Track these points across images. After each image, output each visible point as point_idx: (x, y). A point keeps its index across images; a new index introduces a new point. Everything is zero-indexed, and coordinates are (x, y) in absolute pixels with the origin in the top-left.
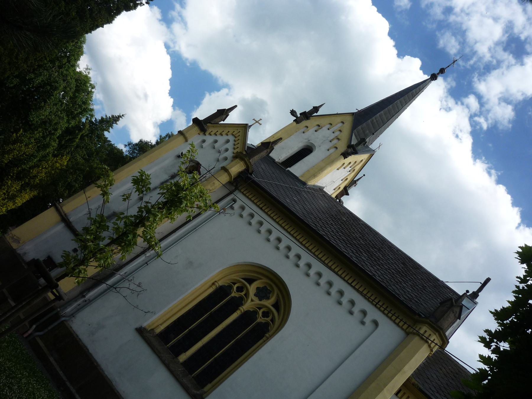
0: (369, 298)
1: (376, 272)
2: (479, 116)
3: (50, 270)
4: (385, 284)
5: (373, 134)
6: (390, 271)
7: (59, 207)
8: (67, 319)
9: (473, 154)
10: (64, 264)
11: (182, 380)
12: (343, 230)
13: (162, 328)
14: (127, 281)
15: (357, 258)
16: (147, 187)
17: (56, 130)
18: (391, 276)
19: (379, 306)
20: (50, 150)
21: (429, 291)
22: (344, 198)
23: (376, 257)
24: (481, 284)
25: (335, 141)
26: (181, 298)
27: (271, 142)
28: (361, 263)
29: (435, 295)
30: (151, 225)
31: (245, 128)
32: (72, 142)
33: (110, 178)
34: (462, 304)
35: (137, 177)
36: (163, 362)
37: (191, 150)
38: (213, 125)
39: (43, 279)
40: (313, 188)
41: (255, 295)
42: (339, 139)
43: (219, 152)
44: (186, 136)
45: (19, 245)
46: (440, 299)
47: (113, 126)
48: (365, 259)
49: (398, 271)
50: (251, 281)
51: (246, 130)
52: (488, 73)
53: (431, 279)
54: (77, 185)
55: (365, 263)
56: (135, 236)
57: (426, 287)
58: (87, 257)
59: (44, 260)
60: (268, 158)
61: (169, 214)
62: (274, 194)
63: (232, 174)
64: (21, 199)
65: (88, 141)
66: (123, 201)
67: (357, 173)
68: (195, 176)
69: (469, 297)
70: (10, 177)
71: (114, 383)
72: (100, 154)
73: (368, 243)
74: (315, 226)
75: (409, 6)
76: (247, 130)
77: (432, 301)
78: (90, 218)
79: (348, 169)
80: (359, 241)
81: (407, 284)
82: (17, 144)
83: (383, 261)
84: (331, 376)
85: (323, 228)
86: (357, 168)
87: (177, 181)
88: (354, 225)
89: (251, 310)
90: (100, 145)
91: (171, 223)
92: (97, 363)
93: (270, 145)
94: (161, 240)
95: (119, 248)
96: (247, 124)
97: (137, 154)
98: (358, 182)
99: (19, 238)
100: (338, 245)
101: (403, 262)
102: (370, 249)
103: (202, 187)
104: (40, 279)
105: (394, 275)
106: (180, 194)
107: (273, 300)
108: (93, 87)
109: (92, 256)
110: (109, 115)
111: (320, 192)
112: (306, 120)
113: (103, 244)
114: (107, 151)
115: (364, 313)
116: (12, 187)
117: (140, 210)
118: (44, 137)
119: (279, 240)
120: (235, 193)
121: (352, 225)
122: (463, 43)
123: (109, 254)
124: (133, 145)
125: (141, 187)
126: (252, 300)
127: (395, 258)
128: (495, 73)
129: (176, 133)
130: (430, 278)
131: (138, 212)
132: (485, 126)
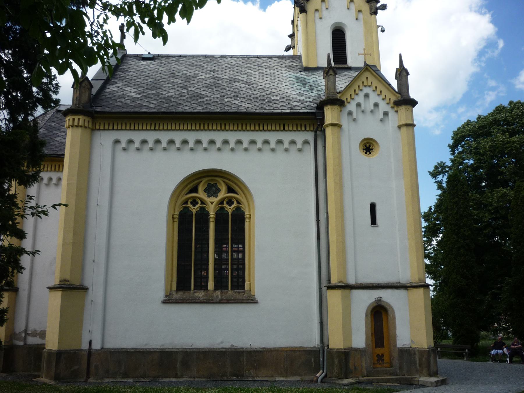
107: (223, 189)
126: (212, 203)
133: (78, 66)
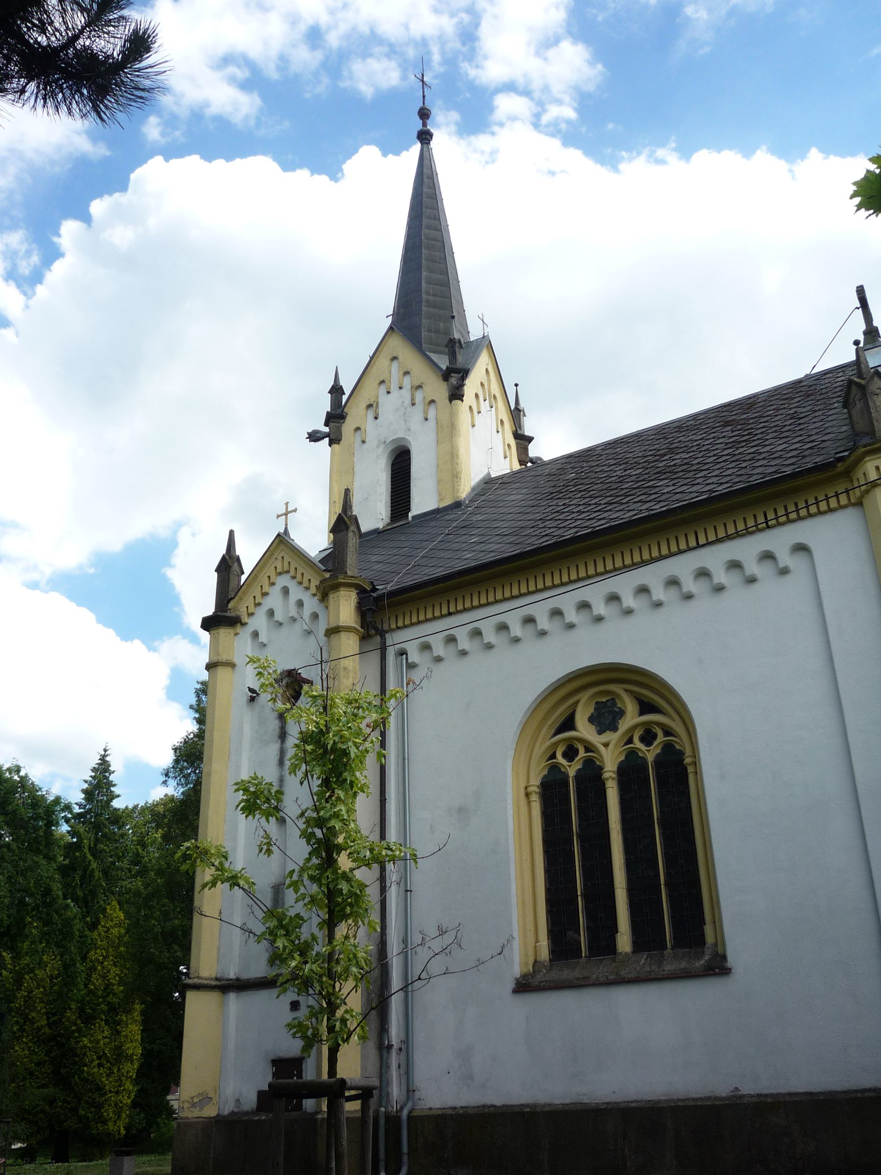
0: (756, 526)
1: (707, 484)
2: (545, 111)
3: (300, 1076)
4: (740, 482)
5: (453, 317)
6: (724, 458)
7: (196, 981)
8: (410, 1105)
9: (605, 167)
10: (311, 1041)
11: (664, 970)
12: (590, 491)
14: (419, 949)
15: (660, 501)
16: (273, 794)
17: (48, 891)
18: (734, 461)
19: (774, 522)
20: (77, 925)
21: (808, 411)
22: (533, 451)
23: (681, 465)
24: (860, 309)
25: (419, 396)
27: (340, 512)
28: (673, 501)
29: (823, 406)
30: (348, 834)
31: (282, 541)
32: (92, 875)
33: (213, 852)
34: (872, 368)
35: (243, 799)
36: (608, 983)
37: (260, 670)
38: (237, 598)
39: (308, 1100)
40: (476, 495)
41: (600, 732)
42: (420, 387)
43: (294, 620)
44: (224, 661)
45: (215, 1103)
46: (837, 402)
47: (112, 781)
48: (672, 488)
49: (732, 442)
50: (568, 724)
51: (288, 545)
52: (477, 44)
53: (788, 393)
54: (177, 922)
55: (679, 493)
56: (347, 878)
57: (796, 412)
58: (328, 991)
59: (274, 1075)
60: (366, 539)
61: (352, 787)
62: (440, 572)
63: (350, 625)
64: (131, 1041)
65: (108, 847)
66: (269, 856)
67: (504, 394)
68: (315, 693)
69: (868, 346)
70: (76, 1035)
71: (586, 1101)
72: (147, 840)
73: (645, 462)
74: (548, 538)
75: (258, 101)
76: (288, 542)
77: (830, 418)
78: (259, 938)
79: (485, 406)
80: (631, 476)
81: (767, 443)
82: (25, 979)
83: (697, 458)
84: (842, 695)
85: (562, 525)
86: (495, 389)
87: (301, 733)
88: (595, 466)
89: (622, 758)
90: (129, 829)
91: (369, 794)
92: (527, 1106)
93: (346, 518)
94: (383, 836)
95: (350, 921)
96: (279, 535)
97: (194, 772)
98: (522, 405)
99: (202, 1093)
100: (611, 519)
101: (722, 423)
102: (658, 467)
103: (342, 695)
104: (304, 1107)
105: (735, 455)
106: (328, 743)
107: (630, 707)
108: (18, 770)
109: (332, 983)
110: (88, 775)
111: (493, 485)
112: (344, 422)
113: (323, 947)
114: (150, 823)
115: (768, 556)
116: (98, 1042)
117: (308, 836)
118: (47, 922)
119: (530, 620)
120: (389, 642)
121: (591, 469)
122: (393, 50)
123: (349, 948)
124: (173, 767)
125: (266, 805)
126: (606, 745)
127: (705, 433)
128: (485, 31)
129: (205, 676)
130: (785, 394)
131: (308, 843)
132: (569, 113)
133: (84, 609)
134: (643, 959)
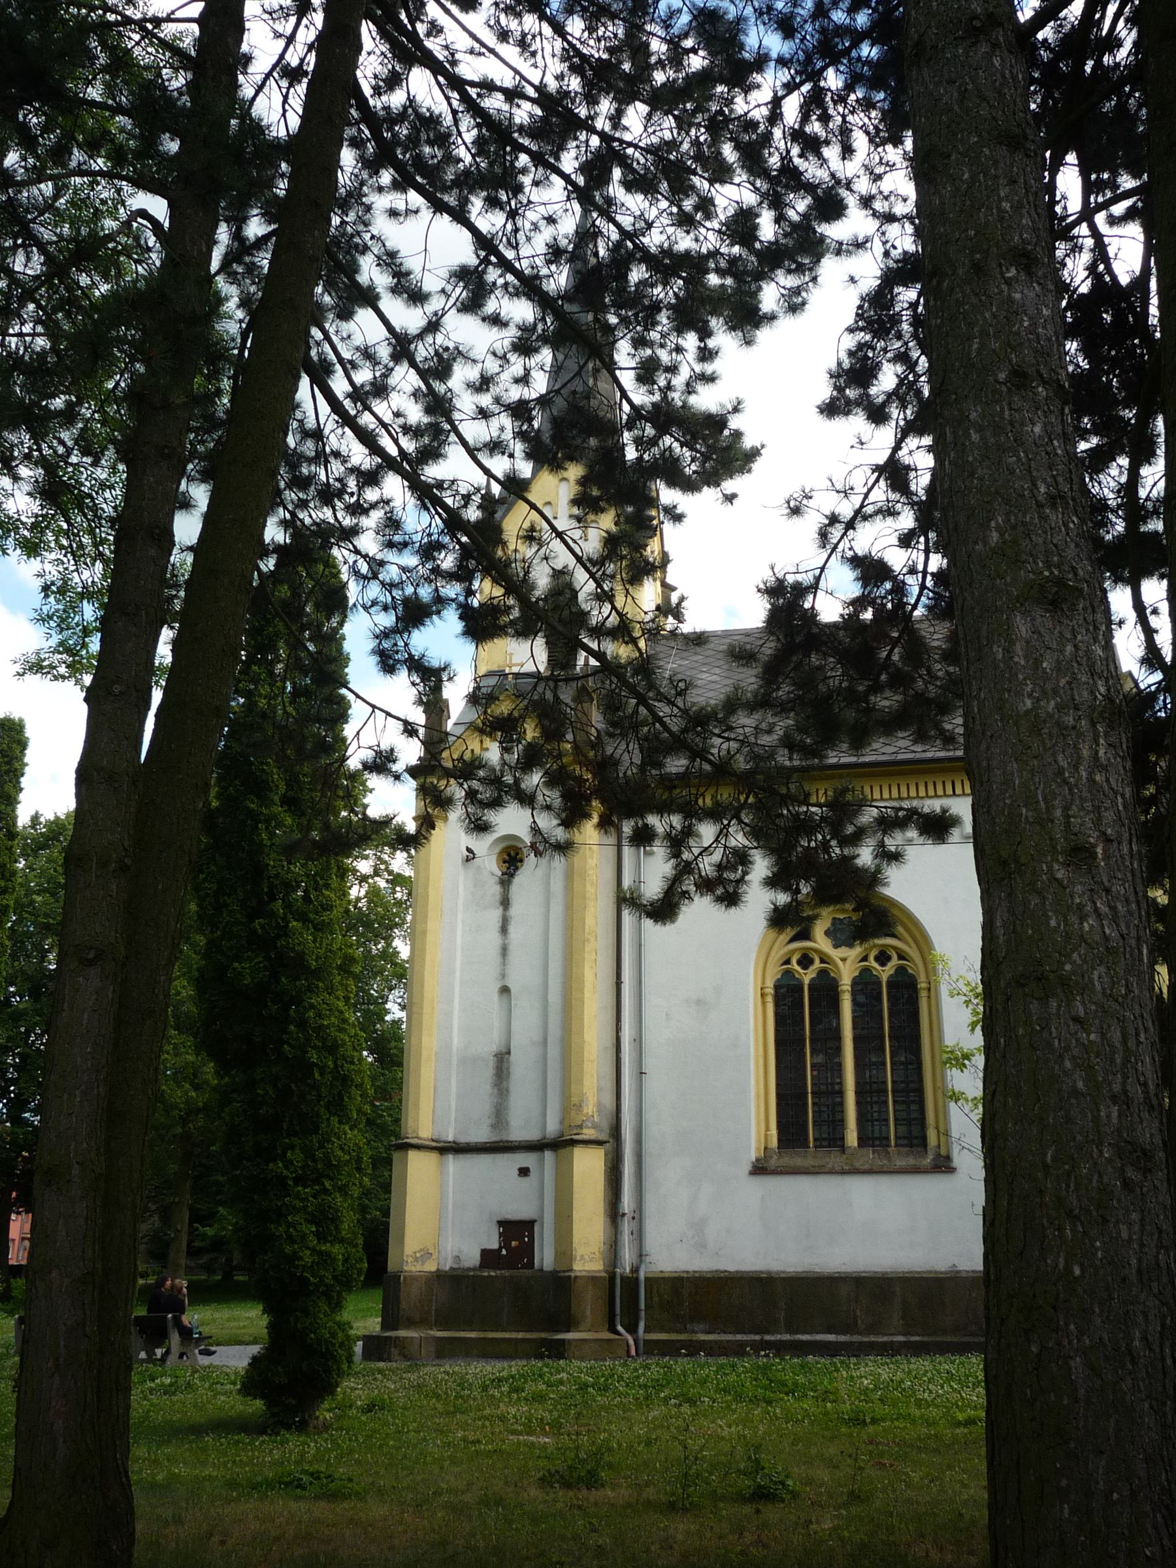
13: (774, 1132)
26: (752, 1067)
36: (843, 1172)
71: (817, 1270)
89: (857, 974)
126: (844, 960)
134: (870, 1153)
